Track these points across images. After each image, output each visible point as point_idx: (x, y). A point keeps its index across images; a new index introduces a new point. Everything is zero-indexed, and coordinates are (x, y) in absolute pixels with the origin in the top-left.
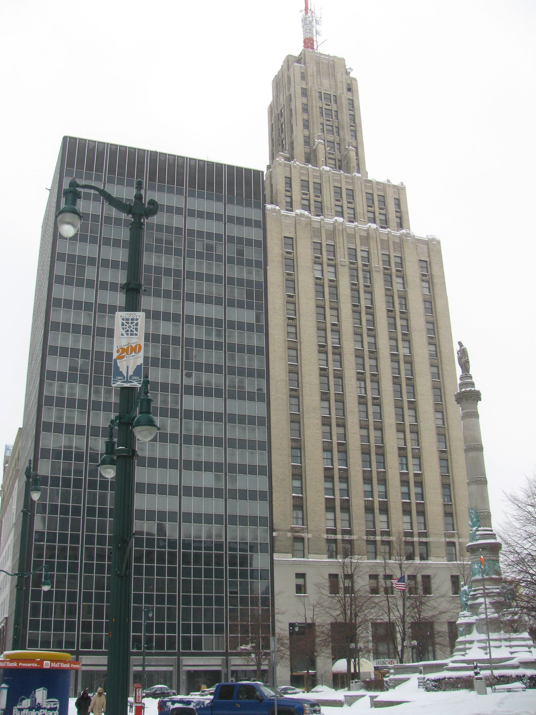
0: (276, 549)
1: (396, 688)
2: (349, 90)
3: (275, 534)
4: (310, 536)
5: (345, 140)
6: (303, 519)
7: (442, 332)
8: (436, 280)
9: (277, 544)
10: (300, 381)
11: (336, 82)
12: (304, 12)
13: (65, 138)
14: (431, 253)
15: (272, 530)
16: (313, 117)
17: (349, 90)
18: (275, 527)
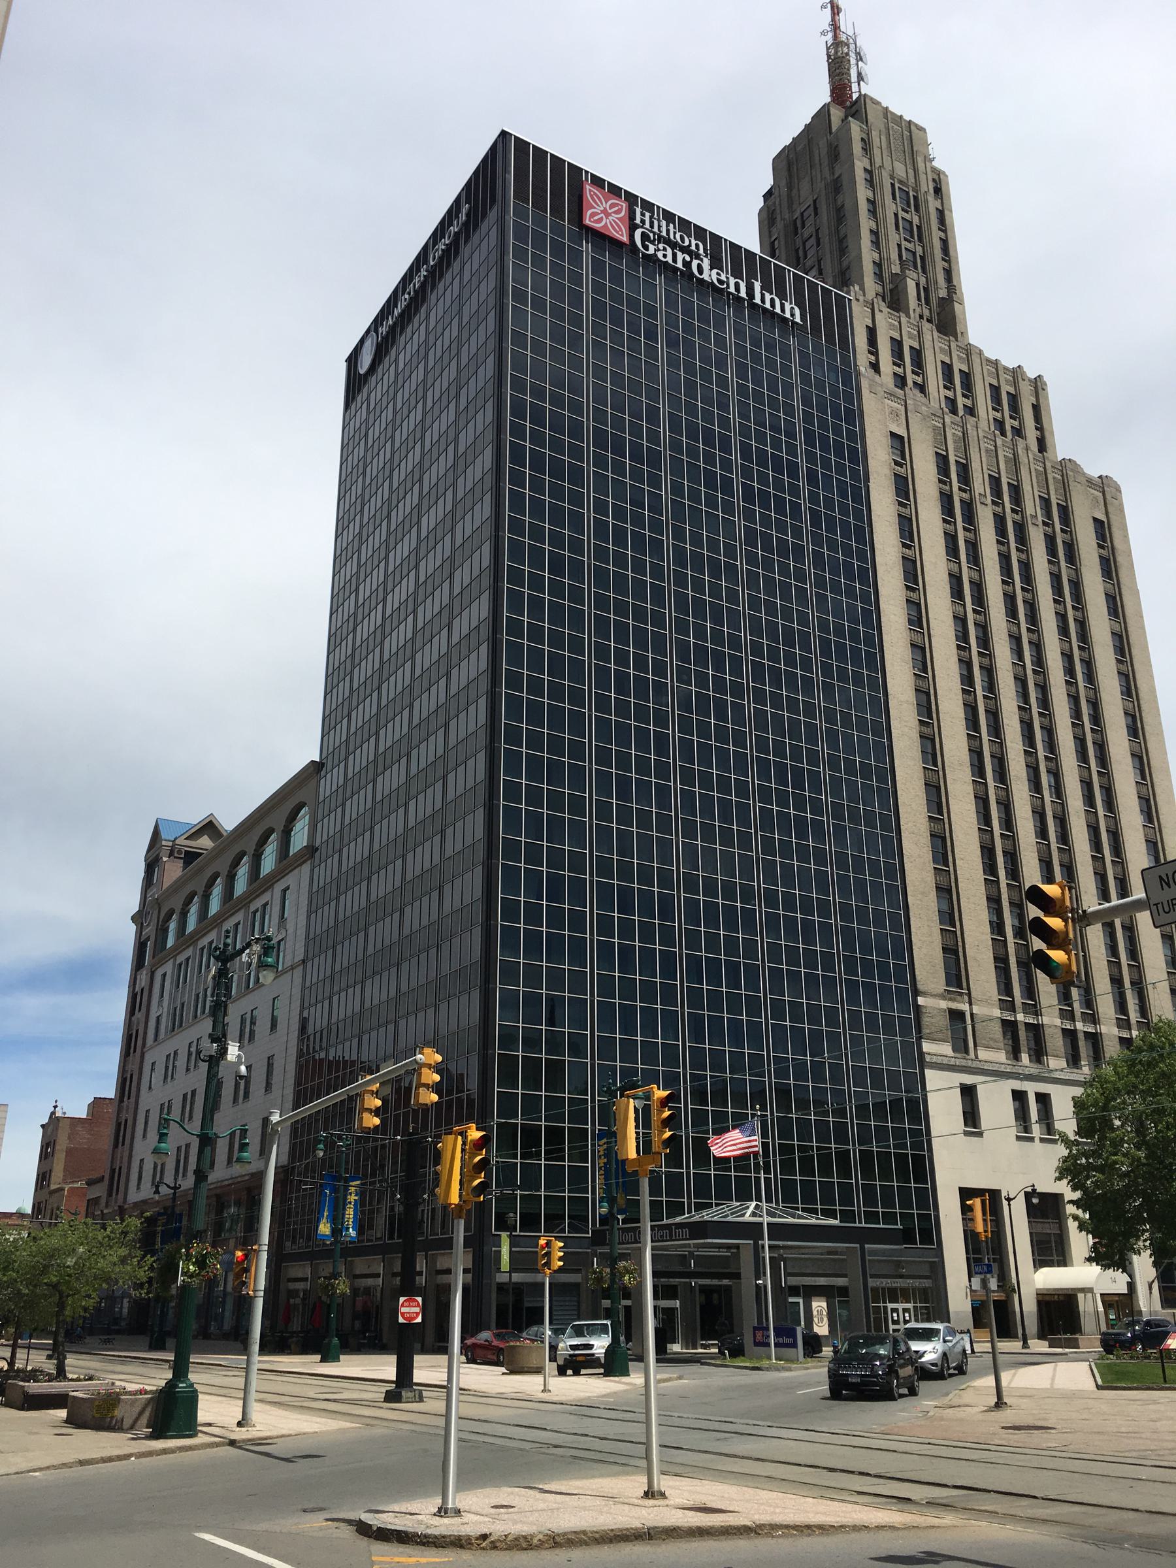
0: (925, 1031)
1: (1011, 365)
9: (926, 1020)
11: (915, 170)
12: (830, 35)
16: (886, 228)
18: (920, 987)
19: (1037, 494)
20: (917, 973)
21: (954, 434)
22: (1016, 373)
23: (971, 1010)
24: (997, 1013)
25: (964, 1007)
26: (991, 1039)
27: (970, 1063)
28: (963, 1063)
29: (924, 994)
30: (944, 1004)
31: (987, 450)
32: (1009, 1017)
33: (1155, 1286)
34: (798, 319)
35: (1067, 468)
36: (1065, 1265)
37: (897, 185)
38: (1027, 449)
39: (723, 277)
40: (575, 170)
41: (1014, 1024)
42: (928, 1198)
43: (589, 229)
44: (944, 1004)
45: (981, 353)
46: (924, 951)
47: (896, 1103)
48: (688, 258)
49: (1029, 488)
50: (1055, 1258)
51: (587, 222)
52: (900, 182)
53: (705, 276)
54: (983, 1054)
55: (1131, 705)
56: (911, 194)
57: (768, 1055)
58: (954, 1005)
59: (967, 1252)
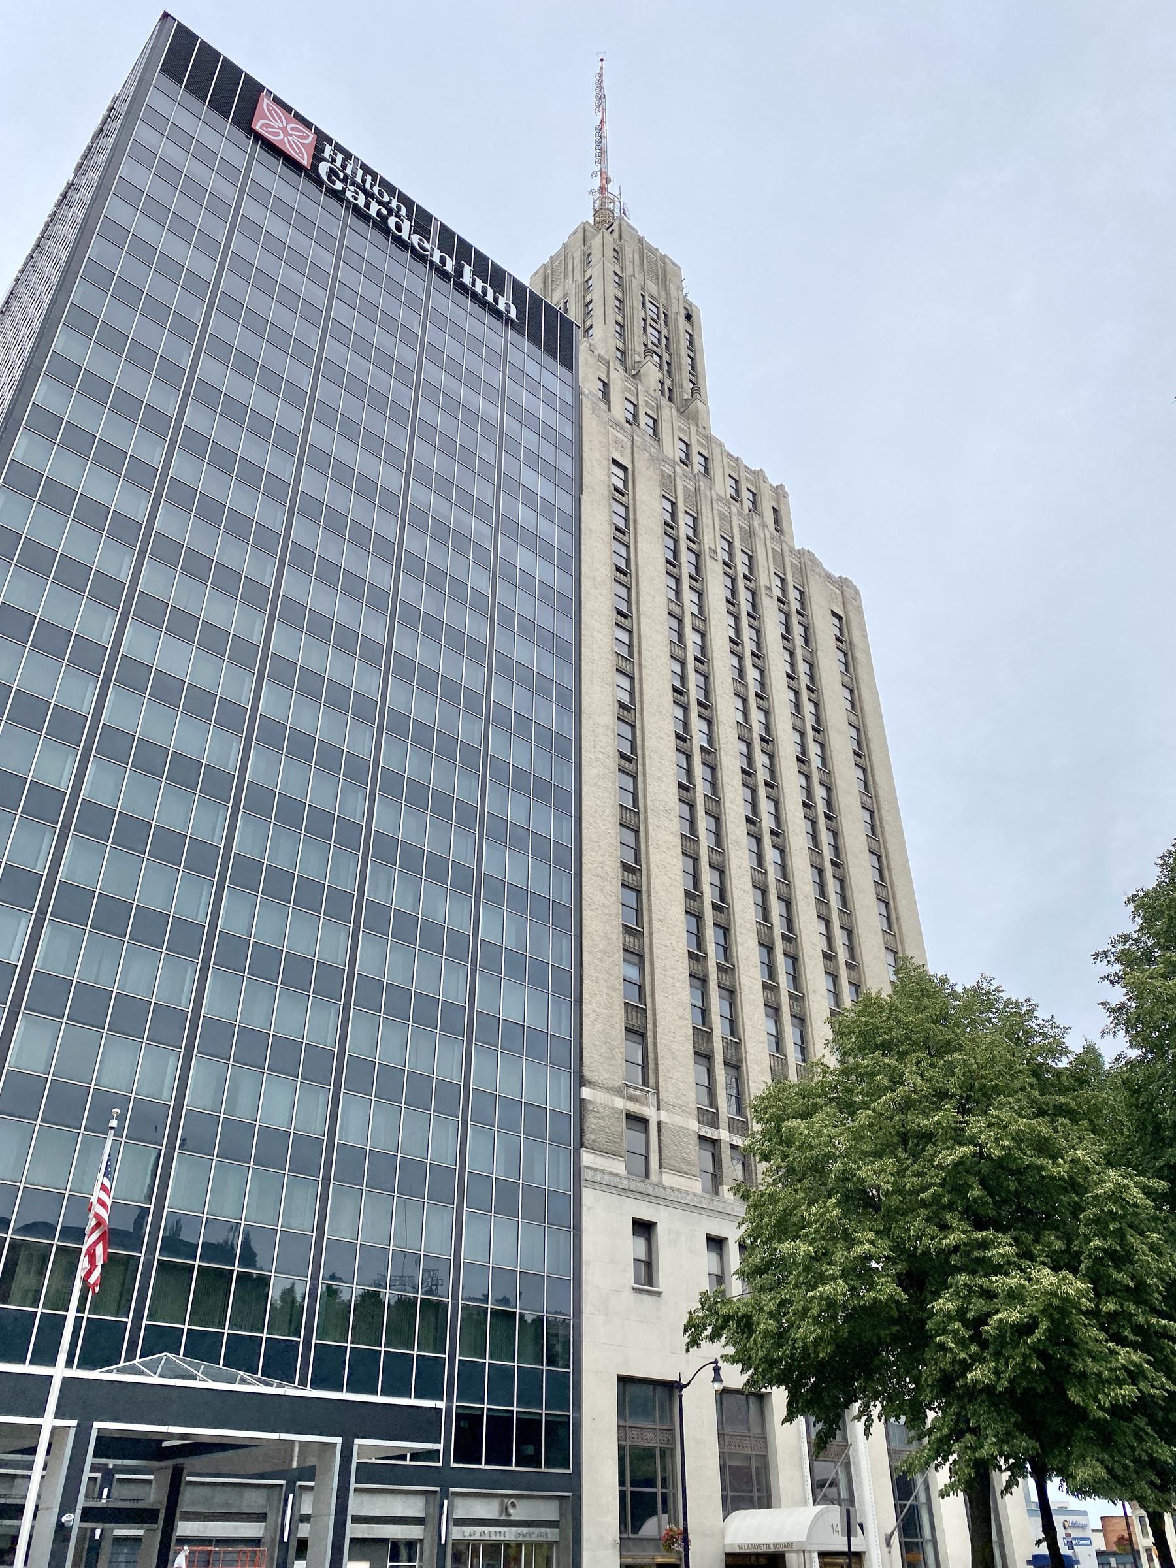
0: (589, 1137)
1: (754, 467)
2: (688, 317)
3: (586, 1092)
4: (664, 1116)
5: (681, 386)
6: (644, 1068)
7: (874, 747)
8: (859, 655)
9: (591, 1122)
10: (639, 742)
13: (166, 15)
14: (849, 607)
15: (581, 1081)
17: (688, 317)
18: (587, 1073)
19: (772, 570)
20: (585, 1054)
21: (684, 487)
22: (758, 475)
23: (658, 1116)
24: (693, 1125)
25: (649, 1112)
26: (684, 1160)
27: (650, 1189)
28: (641, 1187)
29: (593, 1085)
30: (620, 1103)
31: (720, 513)
32: (709, 1132)
33: (896, 1537)
34: (513, 314)
35: (805, 562)
36: (769, 1505)
37: (647, 298)
38: (764, 526)
39: (426, 245)
40: (260, 88)
41: (715, 1143)
42: (565, 1390)
43: (258, 137)
44: (620, 1103)
45: (721, 445)
46: (599, 1026)
47: (529, 1427)
48: (384, 212)
49: (765, 561)
50: (756, 1494)
51: (258, 126)
52: (652, 297)
53: (404, 235)
54: (669, 1179)
55: (868, 800)
56: (662, 310)
57: (308, 1342)
58: (634, 1107)
59: (622, 1483)
